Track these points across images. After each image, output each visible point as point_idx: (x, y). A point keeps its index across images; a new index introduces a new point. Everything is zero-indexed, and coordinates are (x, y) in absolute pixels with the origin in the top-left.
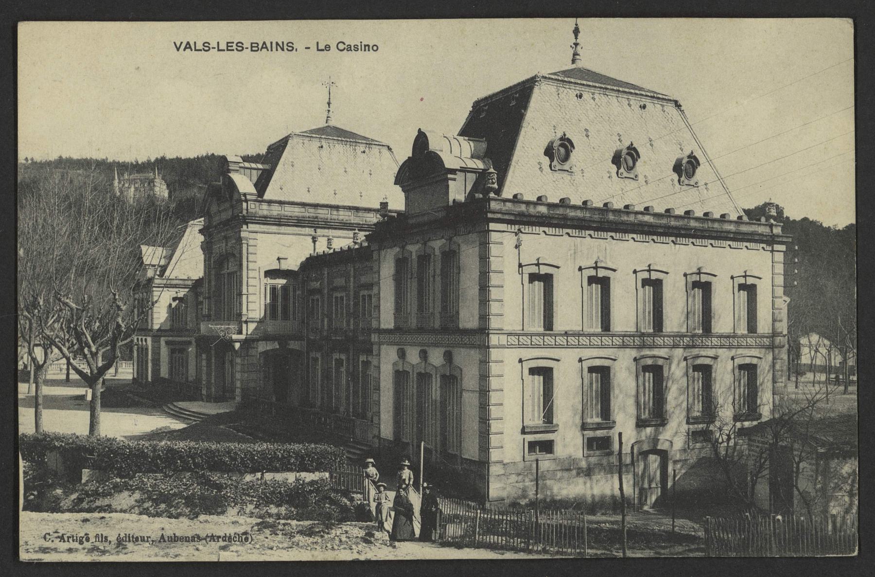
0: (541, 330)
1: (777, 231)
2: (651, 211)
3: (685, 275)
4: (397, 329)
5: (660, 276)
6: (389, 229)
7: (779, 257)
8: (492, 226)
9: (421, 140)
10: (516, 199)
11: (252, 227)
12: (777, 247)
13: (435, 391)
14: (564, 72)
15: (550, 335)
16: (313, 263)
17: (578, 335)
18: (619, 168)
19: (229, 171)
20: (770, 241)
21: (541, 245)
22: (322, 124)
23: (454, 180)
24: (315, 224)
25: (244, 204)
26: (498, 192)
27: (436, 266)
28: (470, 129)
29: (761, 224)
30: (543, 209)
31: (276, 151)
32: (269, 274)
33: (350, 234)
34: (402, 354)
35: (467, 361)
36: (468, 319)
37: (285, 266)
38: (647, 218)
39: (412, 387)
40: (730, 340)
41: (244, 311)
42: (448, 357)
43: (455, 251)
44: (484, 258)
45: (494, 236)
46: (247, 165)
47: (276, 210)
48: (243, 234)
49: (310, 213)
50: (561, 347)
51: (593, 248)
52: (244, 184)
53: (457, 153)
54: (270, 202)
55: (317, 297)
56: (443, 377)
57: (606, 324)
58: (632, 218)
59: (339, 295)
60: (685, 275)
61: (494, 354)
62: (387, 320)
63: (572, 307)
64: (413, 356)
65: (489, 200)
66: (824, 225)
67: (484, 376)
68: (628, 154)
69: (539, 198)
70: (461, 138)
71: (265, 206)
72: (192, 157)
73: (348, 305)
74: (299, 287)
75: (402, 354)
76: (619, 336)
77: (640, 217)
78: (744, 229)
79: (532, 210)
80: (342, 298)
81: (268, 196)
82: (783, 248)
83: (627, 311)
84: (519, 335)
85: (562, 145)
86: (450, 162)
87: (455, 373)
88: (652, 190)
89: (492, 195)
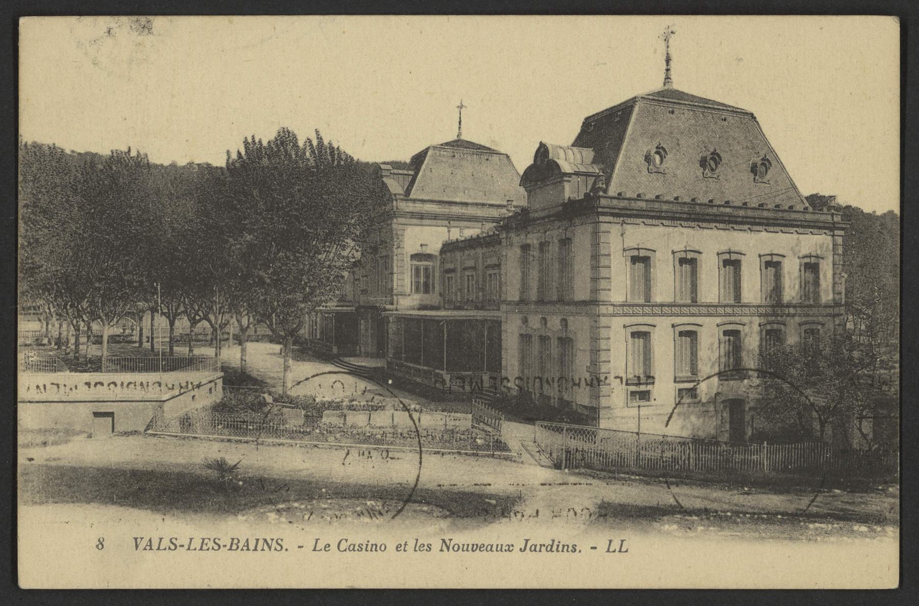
0: (732, 302)
1: (837, 219)
2: (643, 197)
3: (760, 256)
4: (522, 301)
5: (648, 254)
6: (521, 220)
7: (840, 240)
8: (602, 218)
9: (542, 151)
10: (620, 197)
11: (401, 220)
12: (836, 232)
13: (555, 349)
14: (659, 93)
15: (649, 306)
16: (449, 248)
17: (670, 305)
18: (756, 175)
19: (382, 176)
20: (831, 228)
21: (641, 235)
22: (452, 137)
23: (569, 181)
24: (450, 219)
25: (395, 203)
26: (605, 191)
27: (554, 249)
28: (581, 141)
29: (820, 212)
30: (642, 205)
31: (418, 160)
32: (414, 257)
33: (480, 225)
34: (525, 321)
35: (579, 325)
36: (581, 292)
37: (428, 251)
38: (728, 210)
39: (536, 347)
40: (711, 310)
41: (395, 287)
42: (564, 322)
43: (570, 239)
44: (596, 244)
45: (603, 227)
46: (396, 171)
47: (419, 207)
48: (394, 226)
49: (445, 210)
50: (655, 315)
51: (682, 237)
52: (395, 186)
53: (570, 160)
54: (414, 201)
55: (452, 275)
56: (560, 339)
57: (648, 298)
58: (715, 210)
59: (469, 274)
60: (760, 256)
61: (603, 321)
62: (513, 294)
63: (666, 283)
64: (535, 322)
65: (599, 197)
66: (865, 211)
67: (595, 339)
68: (711, 159)
69: (639, 195)
70: (575, 149)
71: (411, 204)
72: (867, 210)
73: (477, 282)
74: (435, 270)
75: (525, 321)
76: (706, 306)
77: (722, 209)
78: (808, 217)
79: (634, 205)
80: (472, 276)
81: (412, 196)
82: (842, 233)
83: (753, 289)
84: (716, 306)
85: (657, 153)
86: (566, 167)
87: (571, 336)
88: (735, 186)
89: (601, 193)
